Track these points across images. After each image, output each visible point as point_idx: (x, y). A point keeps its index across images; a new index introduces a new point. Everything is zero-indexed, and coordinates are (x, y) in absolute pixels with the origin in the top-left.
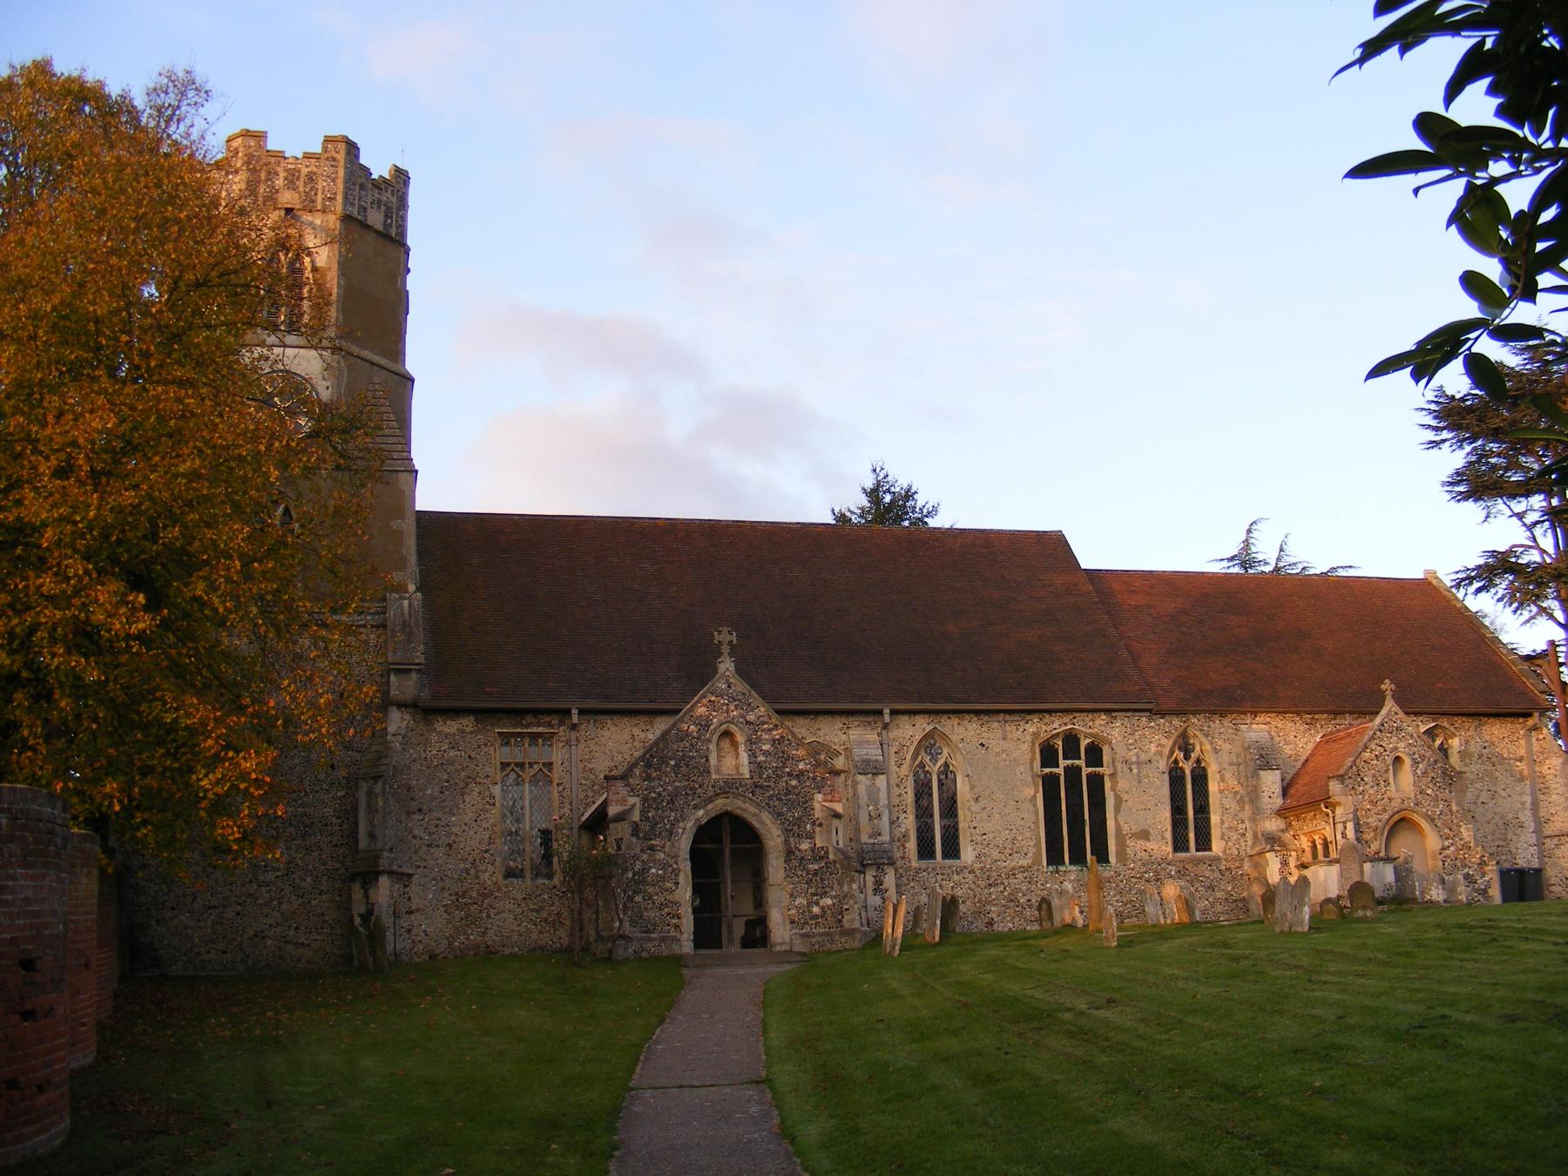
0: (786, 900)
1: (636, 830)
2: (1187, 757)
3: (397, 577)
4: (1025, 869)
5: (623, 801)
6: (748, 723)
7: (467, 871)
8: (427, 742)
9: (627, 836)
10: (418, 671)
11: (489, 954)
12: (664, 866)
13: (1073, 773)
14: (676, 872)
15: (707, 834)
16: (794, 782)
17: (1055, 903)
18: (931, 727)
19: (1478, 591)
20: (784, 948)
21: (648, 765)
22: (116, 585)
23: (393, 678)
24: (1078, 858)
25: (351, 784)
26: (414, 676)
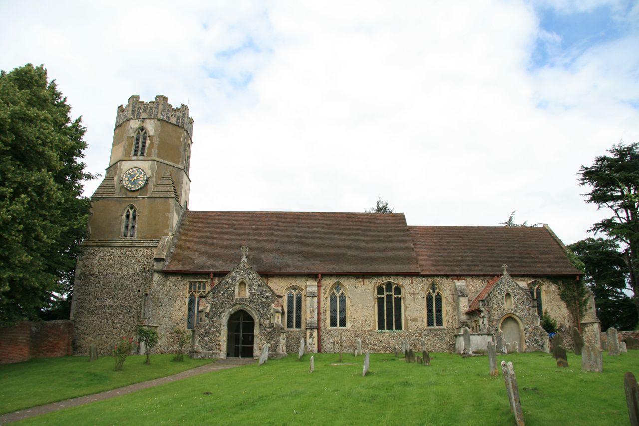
2: (434, 292)
4: (369, 331)
6: (249, 279)
8: (165, 284)
12: (217, 328)
13: (389, 297)
14: (220, 330)
15: (233, 317)
16: (264, 300)
18: (337, 280)
19: (601, 231)
21: (214, 293)
24: (390, 327)
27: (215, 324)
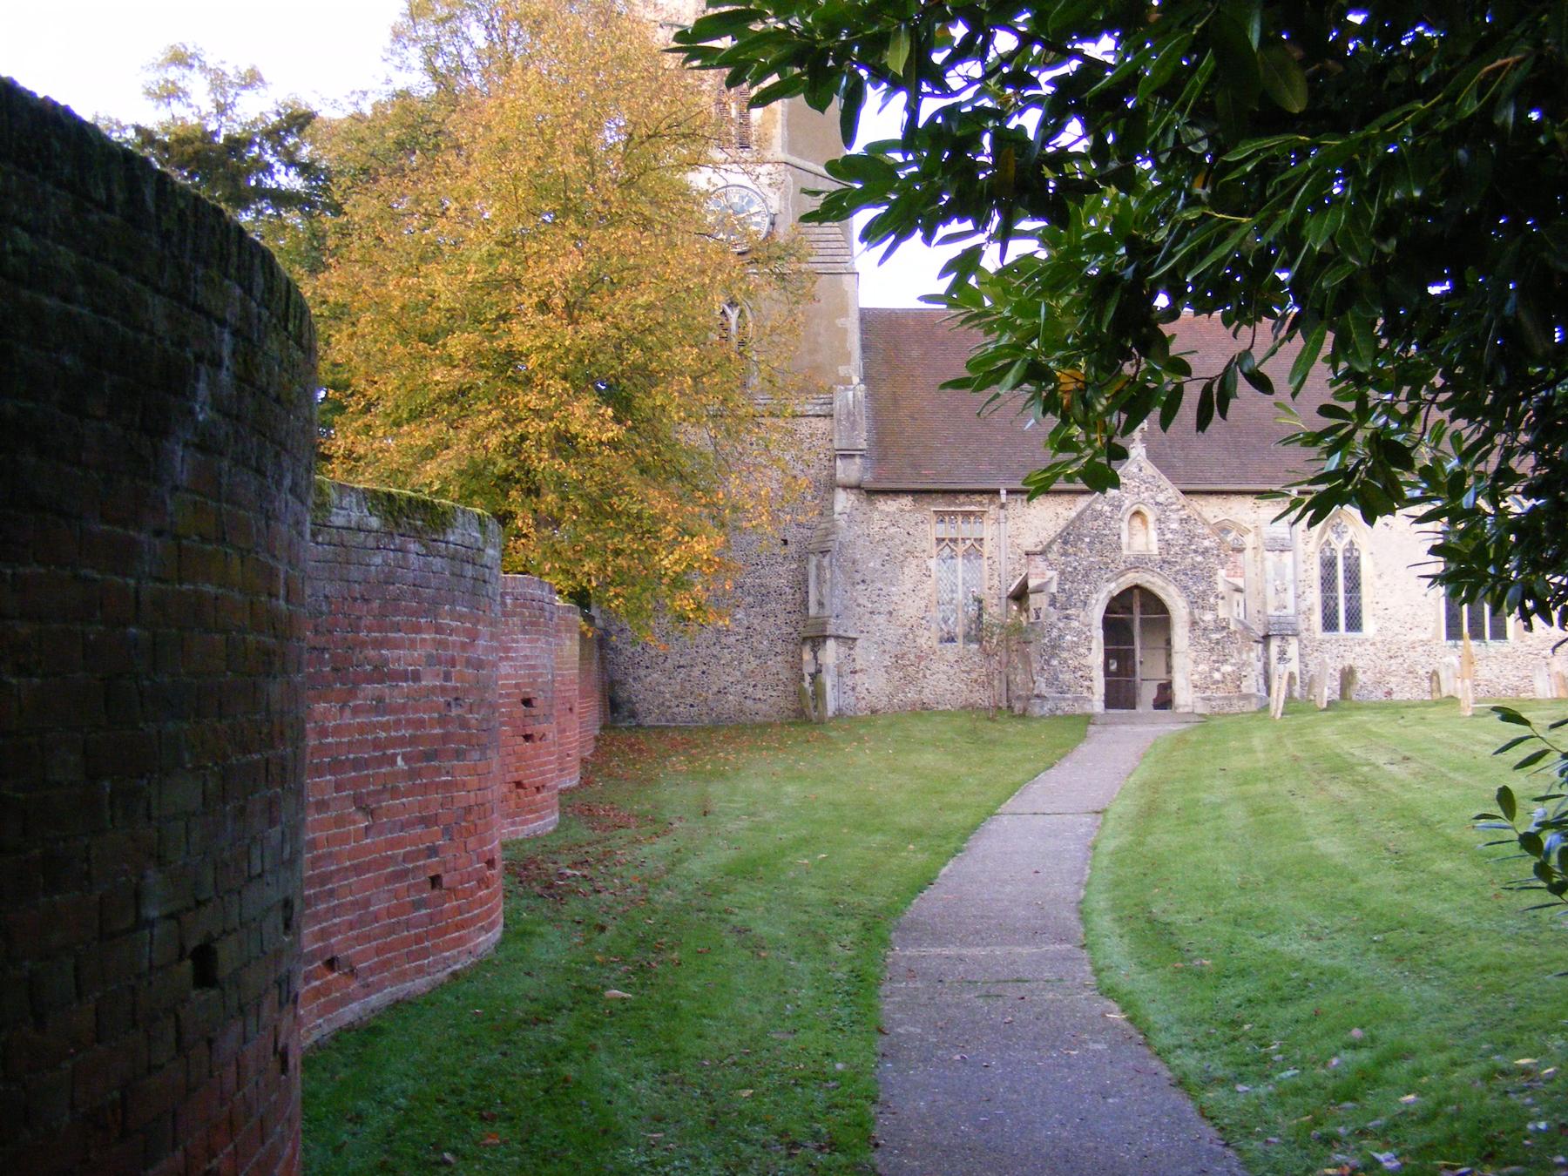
0: (1191, 666)
1: (1053, 603)
3: (842, 370)
4: (1424, 643)
5: (1041, 574)
7: (906, 636)
8: (869, 520)
9: (1045, 606)
10: (862, 456)
11: (922, 710)
12: (1079, 633)
14: (1089, 639)
17: (1442, 675)
20: (1187, 710)
21: (1065, 543)
22: (589, 400)
23: (839, 462)
24: (1477, 634)
25: (803, 558)
26: (858, 460)
27: (1075, 624)
